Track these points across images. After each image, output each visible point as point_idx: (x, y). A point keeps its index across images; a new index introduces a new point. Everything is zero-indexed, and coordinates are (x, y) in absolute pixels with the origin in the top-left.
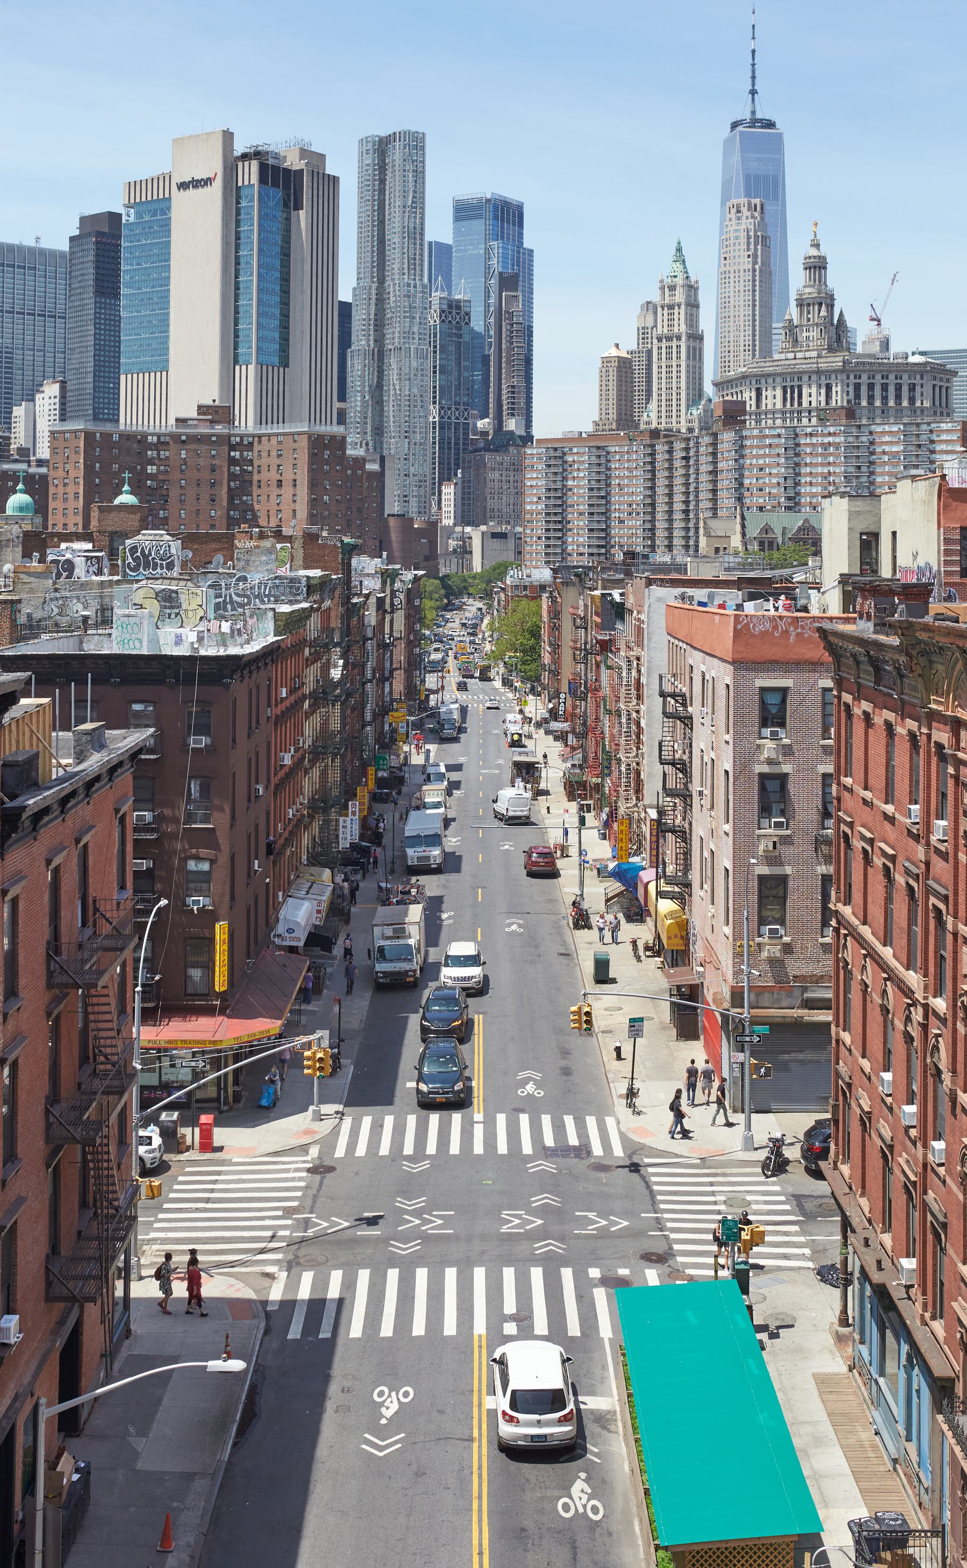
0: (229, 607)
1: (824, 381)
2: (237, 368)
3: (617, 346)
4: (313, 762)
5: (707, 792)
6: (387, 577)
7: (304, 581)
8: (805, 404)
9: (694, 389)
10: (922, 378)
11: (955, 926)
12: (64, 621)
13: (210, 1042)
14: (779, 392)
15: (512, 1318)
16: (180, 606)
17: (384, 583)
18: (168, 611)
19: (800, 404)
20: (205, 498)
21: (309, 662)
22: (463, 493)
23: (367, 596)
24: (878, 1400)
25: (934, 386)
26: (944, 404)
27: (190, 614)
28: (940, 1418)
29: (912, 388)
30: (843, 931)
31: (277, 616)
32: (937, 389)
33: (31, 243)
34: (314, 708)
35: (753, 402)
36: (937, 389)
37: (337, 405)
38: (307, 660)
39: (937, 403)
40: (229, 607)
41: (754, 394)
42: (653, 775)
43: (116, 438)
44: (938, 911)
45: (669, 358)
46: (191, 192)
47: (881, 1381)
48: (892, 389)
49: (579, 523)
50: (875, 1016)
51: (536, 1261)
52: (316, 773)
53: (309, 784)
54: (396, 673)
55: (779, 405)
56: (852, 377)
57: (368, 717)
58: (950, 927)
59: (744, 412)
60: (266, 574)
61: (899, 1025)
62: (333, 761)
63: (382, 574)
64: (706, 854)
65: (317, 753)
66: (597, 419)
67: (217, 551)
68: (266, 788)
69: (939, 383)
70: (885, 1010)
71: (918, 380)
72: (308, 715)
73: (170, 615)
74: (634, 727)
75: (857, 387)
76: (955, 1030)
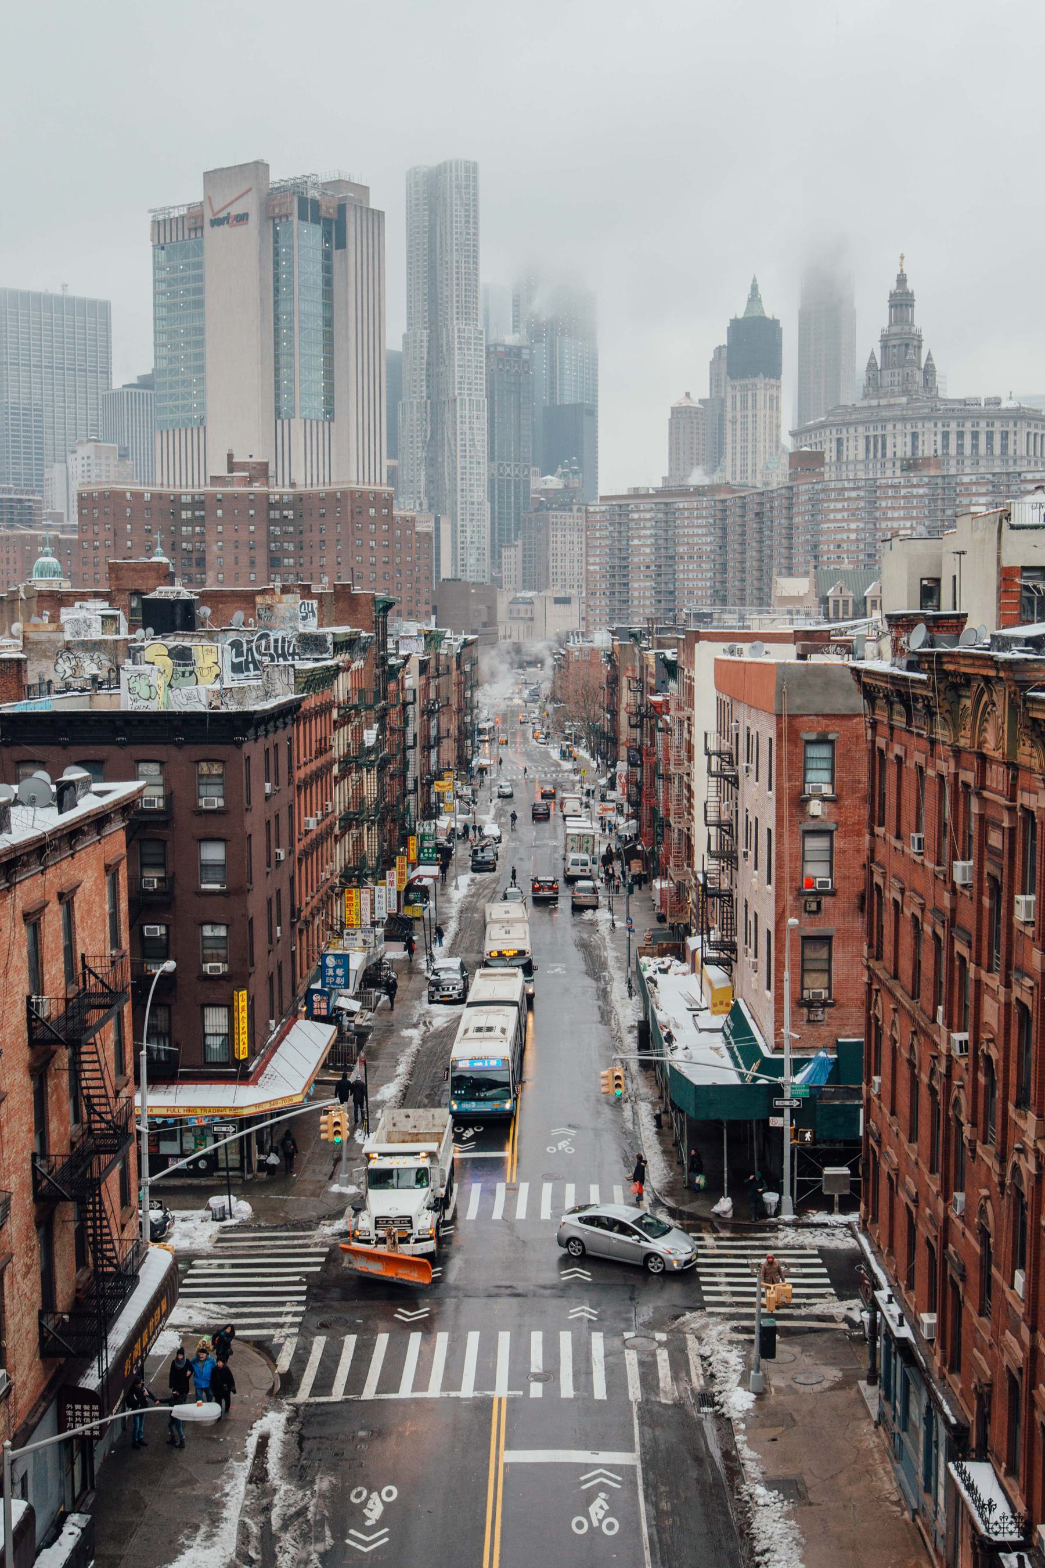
0: (251, 666)
1: (909, 429)
2: (279, 422)
3: (688, 395)
4: (345, 829)
5: (751, 853)
6: (432, 639)
7: (330, 639)
8: (889, 454)
9: (771, 441)
10: (1015, 425)
11: (977, 973)
12: (77, 683)
13: (230, 1108)
14: (862, 443)
15: (537, 1378)
16: (194, 664)
17: (428, 645)
18: (182, 669)
19: (884, 455)
20: (244, 560)
21: (337, 725)
22: (524, 556)
23: (407, 658)
24: (898, 1454)
25: (1028, 434)
26: (1038, 454)
27: (205, 672)
28: (951, 1465)
29: (1005, 436)
30: (875, 986)
31: (297, 673)
32: (1032, 437)
33: (58, 292)
34: (344, 774)
35: (834, 454)
36: (1032, 437)
37: (386, 462)
38: (335, 722)
39: (1032, 453)
40: (251, 666)
41: (834, 445)
42: (702, 837)
43: (147, 497)
44: (963, 959)
45: (744, 408)
46: (225, 229)
47: (904, 1435)
48: (982, 438)
49: (641, 587)
50: (904, 1071)
51: (568, 1326)
52: (348, 840)
53: (340, 855)
54: (445, 741)
55: (861, 456)
56: (940, 425)
57: (410, 785)
58: (972, 975)
59: (822, 463)
60: (290, 631)
61: (924, 1078)
62: (369, 829)
63: (426, 636)
64: (751, 918)
65: (349, 821)
66: (667, 475)
67: (240, 608)
68: (290, 853)
69: (1033, 430)
70: (911, 1064)
71: (1011, 427)
72: (337, 780)
73: (183, 674)
74: (685, 791)
75: (946, 435)
76: (975, 1080)
